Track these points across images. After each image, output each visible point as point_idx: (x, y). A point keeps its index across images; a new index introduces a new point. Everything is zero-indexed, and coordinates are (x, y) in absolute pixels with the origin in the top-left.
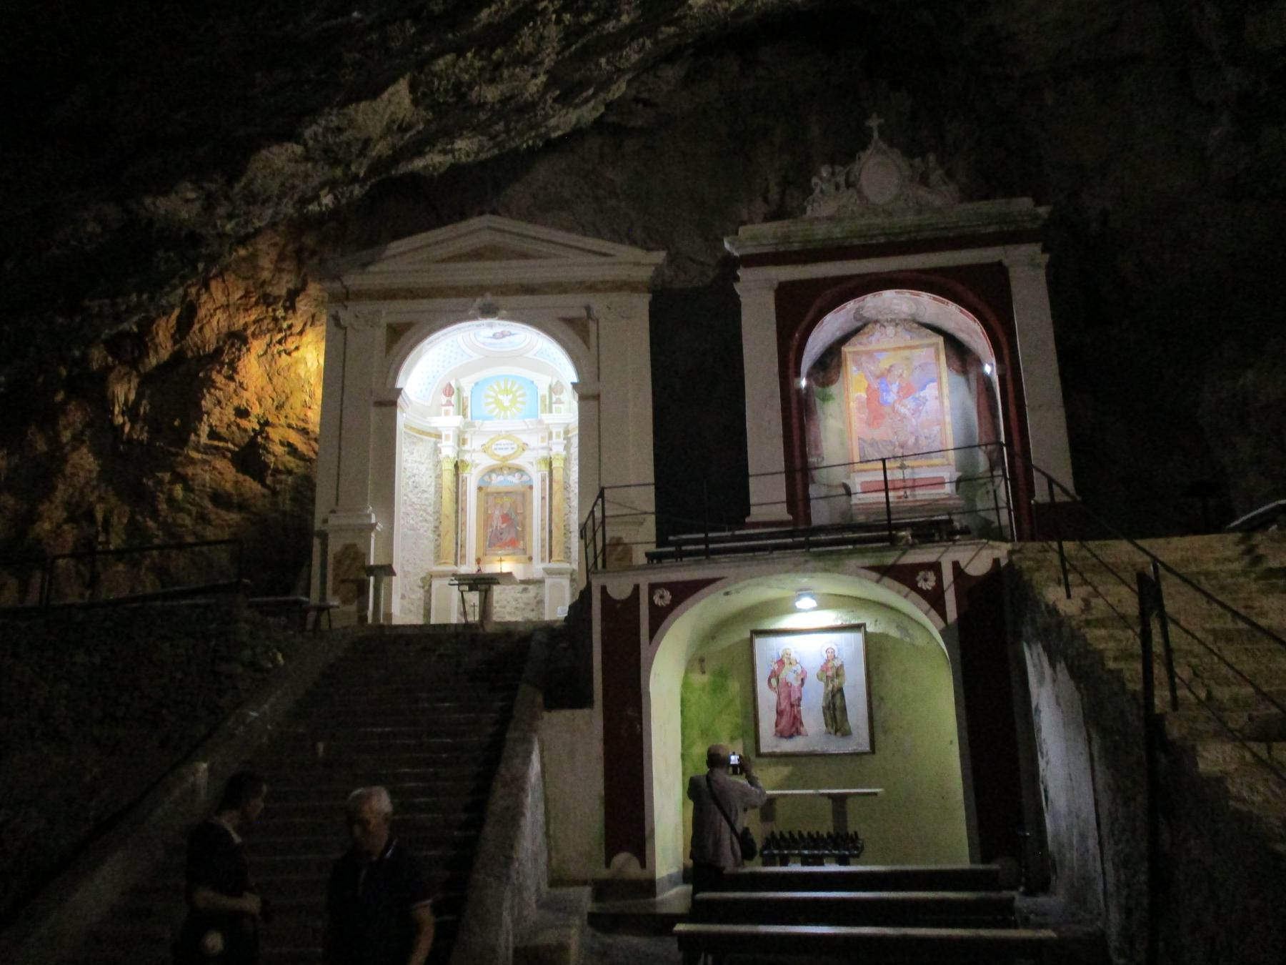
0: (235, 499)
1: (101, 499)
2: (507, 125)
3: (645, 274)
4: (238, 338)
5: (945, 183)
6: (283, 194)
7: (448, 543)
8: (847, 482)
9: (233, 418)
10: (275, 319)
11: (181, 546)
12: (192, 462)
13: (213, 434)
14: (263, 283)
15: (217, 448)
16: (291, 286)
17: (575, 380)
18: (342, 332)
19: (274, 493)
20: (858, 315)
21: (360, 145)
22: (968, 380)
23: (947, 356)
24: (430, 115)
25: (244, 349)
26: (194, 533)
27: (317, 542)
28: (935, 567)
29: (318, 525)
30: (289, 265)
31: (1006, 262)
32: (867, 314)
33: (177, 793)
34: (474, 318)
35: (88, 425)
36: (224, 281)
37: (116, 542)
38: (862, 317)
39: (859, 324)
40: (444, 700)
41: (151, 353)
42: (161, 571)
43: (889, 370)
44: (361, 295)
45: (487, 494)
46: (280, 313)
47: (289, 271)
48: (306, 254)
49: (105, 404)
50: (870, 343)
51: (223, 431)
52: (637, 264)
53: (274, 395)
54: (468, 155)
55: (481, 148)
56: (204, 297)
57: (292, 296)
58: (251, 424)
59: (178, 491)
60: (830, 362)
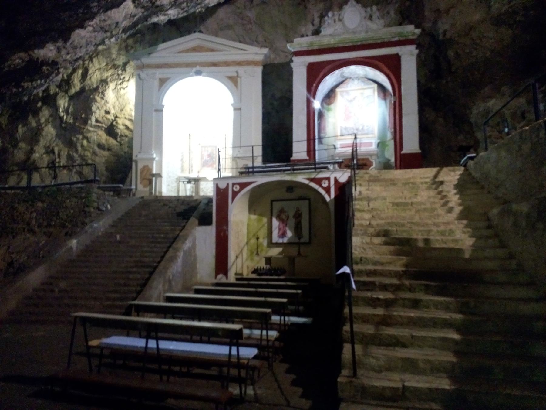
0: (106, 147)
1: (57, 145)
2: (187, 4)
3: (260, 58)
4: (104, 82)
5: (379, 19)
6: (87, 44)
7: (186, 166)
8: (334, 144)
9: (104, 114)
10: (118, 75)
11: (87, 164)
12: (89, 131)
13: (97, 121)
14: (113, 60)
15: (99, 126)
16: (124, 61)
19: (121, 145)
21: (115, 25)
22: (386, 103)
23: (378, 92)
24: (143, 10)
25: (107, 87)
26: (92, 160)
27: (134, 164)
28: (328, 179)
29: (134, 158)
30: (123, 52)
31: (400, 54)
33: (64, 249)
34: (192, 76)
35: (51, 116)
37: (63, 162)
38: (344, 77)
39: (344, 79)
40: (165, 222)
41: (72, 88)
42: (80, 173)
43: (354, 99)
44: (149, 66)
46: (120, 72)
48: (129, 48)
49: (56, 108)
50: (347, 87)
51: (100, 119)
52: (257, 54)
54: (174, 16)
55: (179, 13)
56: (91, 65)
57: (125, 65)
58: (111, 117)
59: (85, 142)
60: (330, 96)
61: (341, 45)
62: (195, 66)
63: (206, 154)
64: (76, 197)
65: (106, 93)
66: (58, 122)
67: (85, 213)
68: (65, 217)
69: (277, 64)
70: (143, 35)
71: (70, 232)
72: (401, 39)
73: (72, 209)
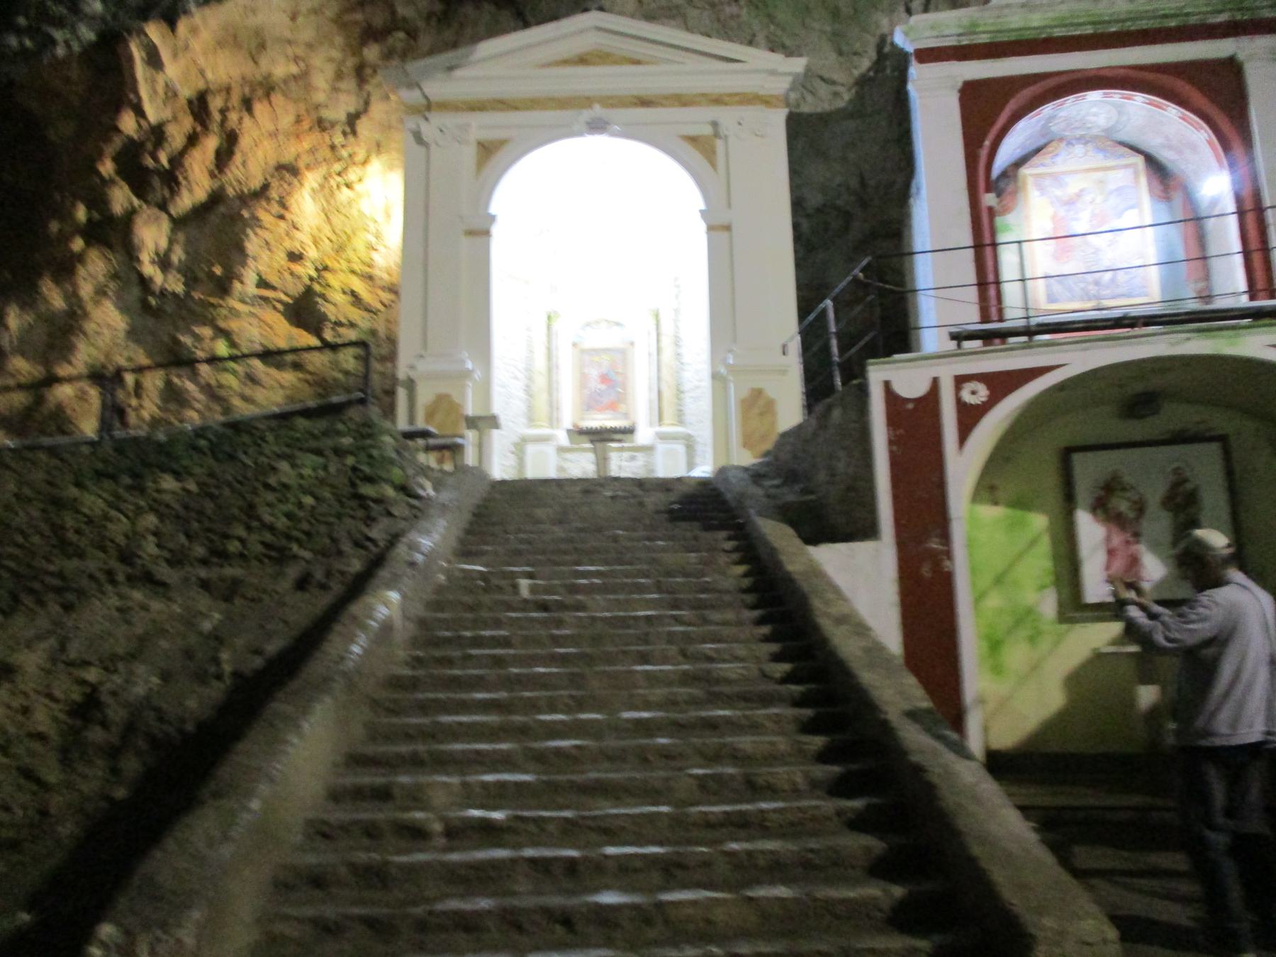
3: (780, 86)
4: (289, 170)
12: (235, 314)
13: (263, 283)
14: (317, 107)
15: (265, 299)
16: (352, 110)
17: (703, 207)
18: (423, 150)
20: (1045, 131)
27: (402, 394)
29: (402, 373)
30: (349, 84)
31: (1241, 56)
32: (1055, 128)
34: (580, 134)
35: (115, 276)
36: (270, 103)
44: (445, 106)
45: (583, 351)
46: (338, 139)
47: (348, 92)
49: (130, 252)
51: (273, 279)
52: (773, 73)
53: (334, 238)
57: (352, 119)
58: (306, 270)
61: (1058, 32)
62: (590, 106)
63: (594, 373)
64: (319, 452)
65: (292, 202)
66: (136, 291)
67: (364, 507)
68: (281, 523)
69: (811, 115)
70: (412, 34)
71: (319, 575)
72: (1239, 17)
73: (307, 492)
